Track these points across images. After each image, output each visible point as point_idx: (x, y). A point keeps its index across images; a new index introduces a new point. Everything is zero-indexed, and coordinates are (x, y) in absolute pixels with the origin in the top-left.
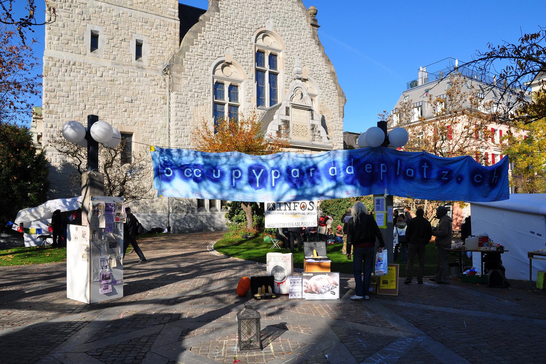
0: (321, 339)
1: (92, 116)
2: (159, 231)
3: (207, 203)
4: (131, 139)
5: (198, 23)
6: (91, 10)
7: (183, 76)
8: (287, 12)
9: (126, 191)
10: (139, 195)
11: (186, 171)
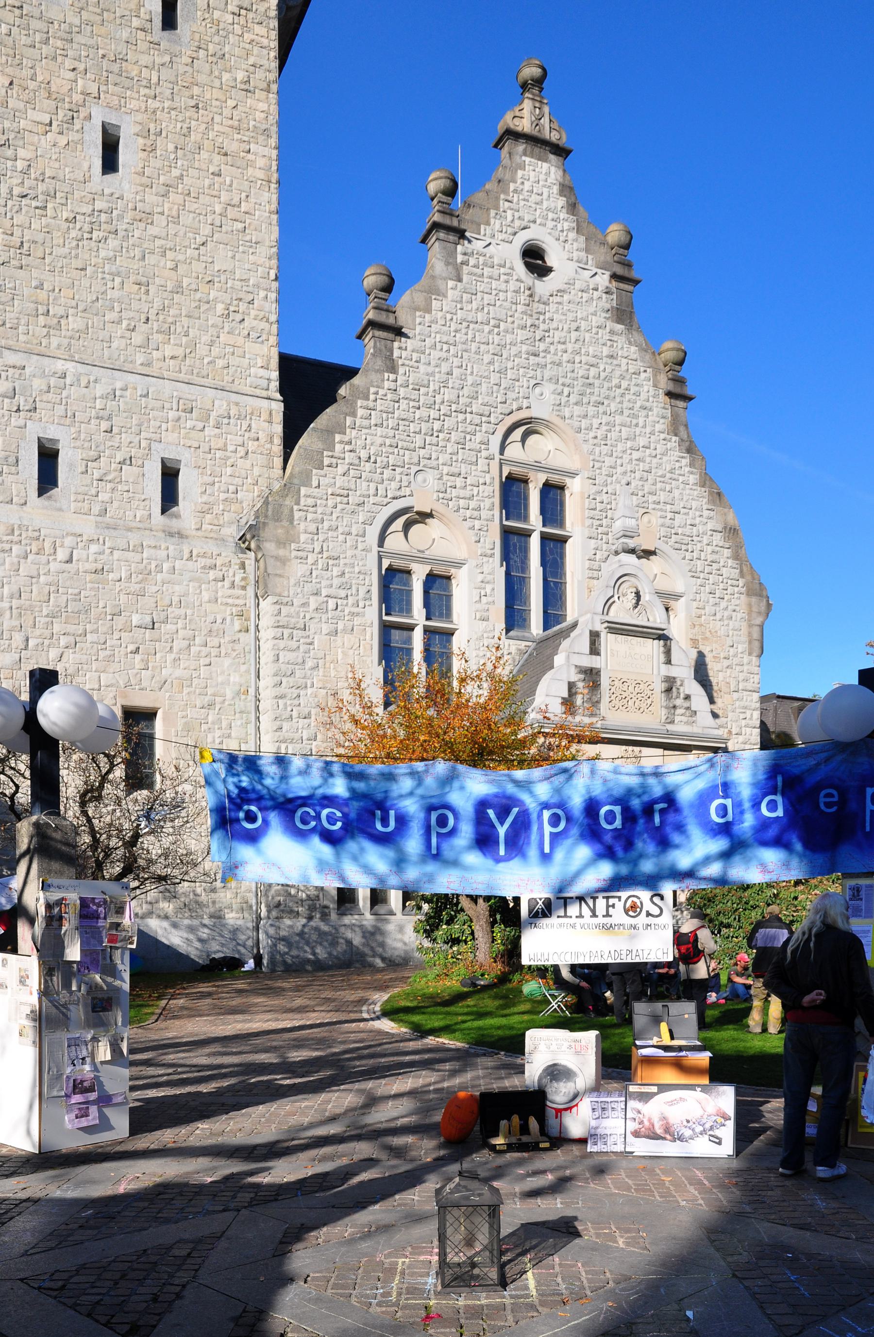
0: (679, 1267)
1: (42, 670)
2: (232, 964)
3: (363, 896)
4: (153, 728)
5: (334, 406)
6: (38, 384)
7: (294, 553)
8: (594, 361)
9: (141, 862)
10: (176, 872)
11: (299, 813)
